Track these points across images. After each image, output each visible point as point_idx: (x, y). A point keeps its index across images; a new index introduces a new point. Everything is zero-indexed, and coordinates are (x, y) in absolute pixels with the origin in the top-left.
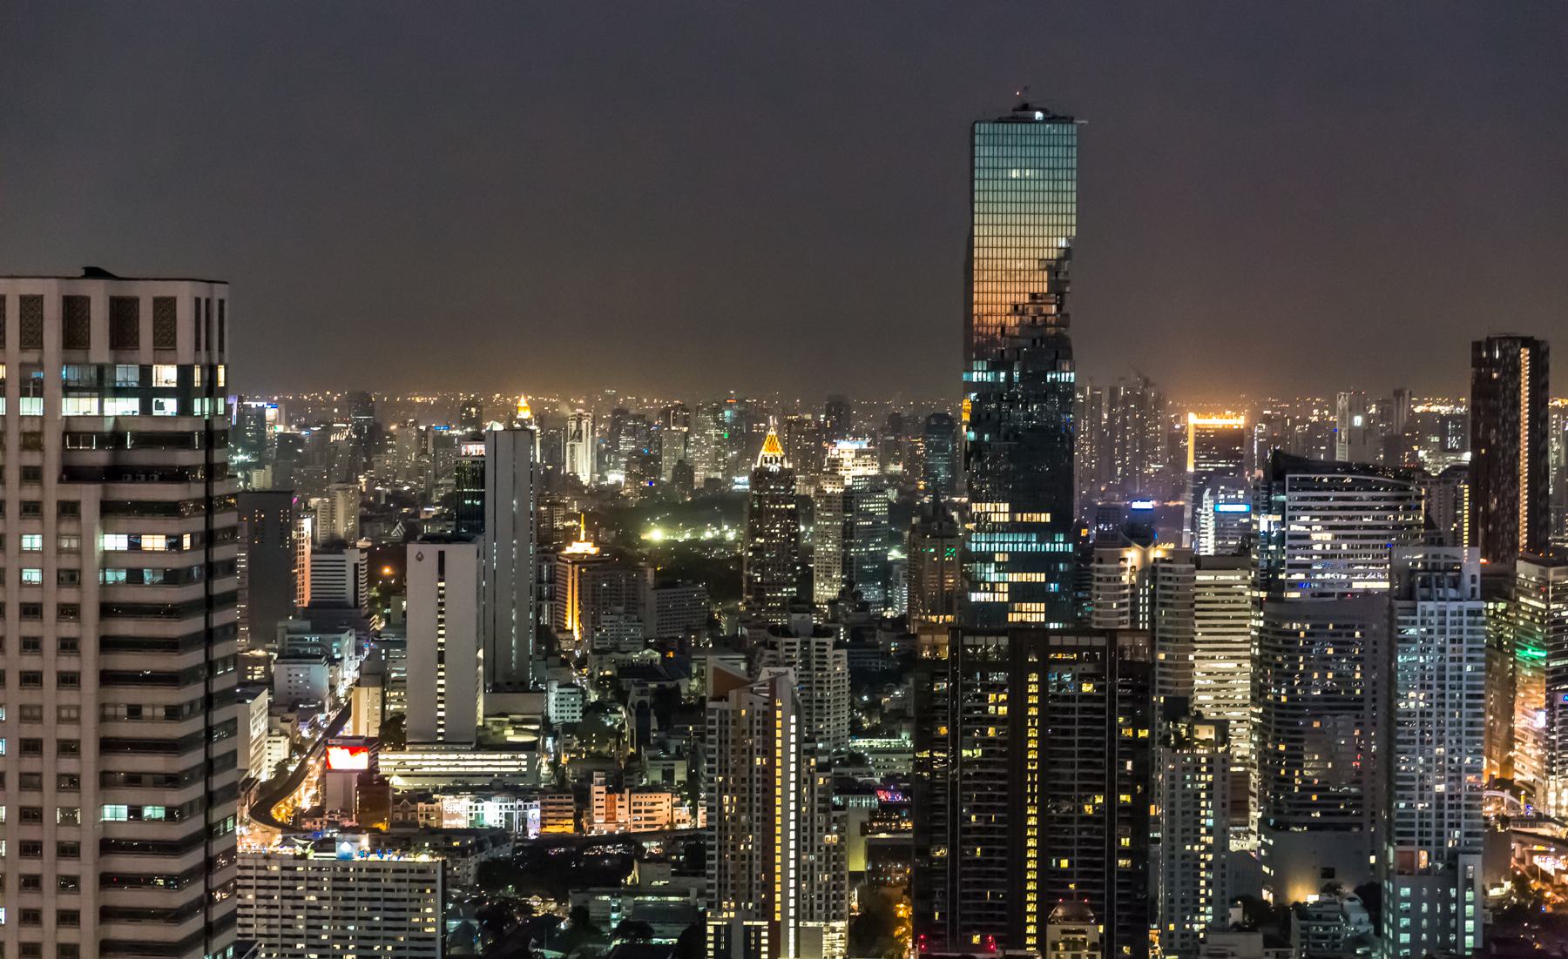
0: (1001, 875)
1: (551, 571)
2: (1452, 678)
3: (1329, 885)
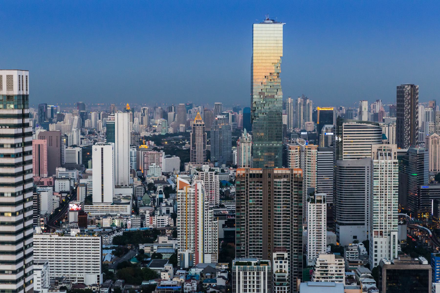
0: (260, 239)
1: (338, 153)
2: (389, 182)
3: (355, 241)
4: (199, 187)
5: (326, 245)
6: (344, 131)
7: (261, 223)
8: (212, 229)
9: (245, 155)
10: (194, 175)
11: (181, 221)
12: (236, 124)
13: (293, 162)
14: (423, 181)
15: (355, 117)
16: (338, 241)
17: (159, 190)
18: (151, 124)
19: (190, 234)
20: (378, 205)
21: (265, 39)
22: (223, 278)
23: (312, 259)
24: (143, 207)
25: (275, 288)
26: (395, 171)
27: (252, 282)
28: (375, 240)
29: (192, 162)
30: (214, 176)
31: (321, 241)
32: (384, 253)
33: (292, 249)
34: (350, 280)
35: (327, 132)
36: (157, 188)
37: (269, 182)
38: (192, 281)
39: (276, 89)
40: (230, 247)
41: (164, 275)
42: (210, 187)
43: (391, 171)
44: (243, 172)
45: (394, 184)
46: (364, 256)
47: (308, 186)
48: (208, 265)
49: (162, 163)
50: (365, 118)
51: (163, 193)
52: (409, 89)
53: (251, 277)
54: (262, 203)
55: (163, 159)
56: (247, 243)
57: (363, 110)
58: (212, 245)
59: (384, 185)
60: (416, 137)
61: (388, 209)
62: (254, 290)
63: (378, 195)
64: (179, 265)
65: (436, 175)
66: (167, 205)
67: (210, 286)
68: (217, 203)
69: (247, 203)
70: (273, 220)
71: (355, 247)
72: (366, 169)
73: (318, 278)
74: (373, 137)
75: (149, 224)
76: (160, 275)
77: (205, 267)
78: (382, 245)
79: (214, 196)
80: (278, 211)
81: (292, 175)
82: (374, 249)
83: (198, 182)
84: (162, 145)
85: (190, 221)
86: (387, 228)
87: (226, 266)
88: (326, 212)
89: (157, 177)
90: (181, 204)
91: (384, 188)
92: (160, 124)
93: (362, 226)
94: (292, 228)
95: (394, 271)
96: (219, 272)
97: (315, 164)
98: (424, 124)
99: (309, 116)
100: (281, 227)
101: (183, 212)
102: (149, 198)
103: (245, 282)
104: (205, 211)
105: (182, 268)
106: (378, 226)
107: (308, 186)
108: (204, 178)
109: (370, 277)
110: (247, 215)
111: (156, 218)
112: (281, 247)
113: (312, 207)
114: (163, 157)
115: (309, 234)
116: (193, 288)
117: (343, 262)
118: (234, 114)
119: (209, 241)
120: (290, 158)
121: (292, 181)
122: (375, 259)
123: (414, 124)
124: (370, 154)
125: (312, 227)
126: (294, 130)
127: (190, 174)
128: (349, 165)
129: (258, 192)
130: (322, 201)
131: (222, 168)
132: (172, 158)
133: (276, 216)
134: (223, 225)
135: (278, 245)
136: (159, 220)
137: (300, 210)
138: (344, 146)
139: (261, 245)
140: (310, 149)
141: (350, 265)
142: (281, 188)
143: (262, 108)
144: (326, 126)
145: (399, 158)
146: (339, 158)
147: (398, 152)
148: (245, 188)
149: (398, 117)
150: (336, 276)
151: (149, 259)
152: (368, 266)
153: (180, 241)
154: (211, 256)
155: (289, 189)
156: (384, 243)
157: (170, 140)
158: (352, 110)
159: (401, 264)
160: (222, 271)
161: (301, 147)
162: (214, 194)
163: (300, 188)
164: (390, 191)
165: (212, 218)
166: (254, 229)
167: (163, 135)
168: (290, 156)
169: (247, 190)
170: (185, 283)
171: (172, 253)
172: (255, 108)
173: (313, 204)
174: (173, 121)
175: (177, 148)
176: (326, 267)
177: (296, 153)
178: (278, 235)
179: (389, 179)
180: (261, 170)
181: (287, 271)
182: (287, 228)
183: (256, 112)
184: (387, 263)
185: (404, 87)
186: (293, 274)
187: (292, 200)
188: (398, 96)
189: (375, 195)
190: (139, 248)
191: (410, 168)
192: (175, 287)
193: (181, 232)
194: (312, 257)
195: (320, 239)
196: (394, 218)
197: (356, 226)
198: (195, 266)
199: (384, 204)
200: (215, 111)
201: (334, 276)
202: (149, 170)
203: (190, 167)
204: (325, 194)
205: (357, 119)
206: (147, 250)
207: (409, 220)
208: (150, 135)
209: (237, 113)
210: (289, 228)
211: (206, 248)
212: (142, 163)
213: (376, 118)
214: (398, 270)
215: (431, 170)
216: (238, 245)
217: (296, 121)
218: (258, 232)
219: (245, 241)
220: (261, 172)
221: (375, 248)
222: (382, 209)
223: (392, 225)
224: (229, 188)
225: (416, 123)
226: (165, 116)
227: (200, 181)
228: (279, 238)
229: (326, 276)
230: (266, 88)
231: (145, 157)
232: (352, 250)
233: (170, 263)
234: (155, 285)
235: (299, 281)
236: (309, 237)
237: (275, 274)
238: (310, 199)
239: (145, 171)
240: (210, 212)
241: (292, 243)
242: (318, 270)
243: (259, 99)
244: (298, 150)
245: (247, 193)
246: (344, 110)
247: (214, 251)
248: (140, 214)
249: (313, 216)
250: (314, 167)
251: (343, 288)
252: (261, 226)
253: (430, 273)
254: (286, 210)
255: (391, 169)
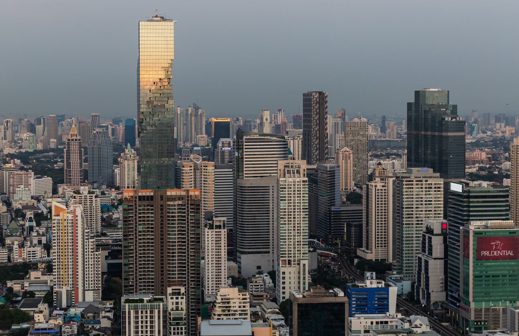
0: (152, 271)
1: (238, 171)
2: (298, 203)
4: (79, 211)
5: (226, 277)
6: (245, 145)
7: (152, 253)
8: (94, 261)
9: (128, 175)
10: (71, 199)
11: (58, 252)
12: (117, 139)
13: (186, 182)
14: (335, 202)
15: (254, 129)
16: (239, 272)
17: (29, 216)
18: (16, 139)
19: (68, 268)
20: (285, 230)
21: (154, 39)
22: (109, 318)
23: (210, 293)
24: (9, 238)
25: (170, 328)
26: (305, 191)
27: (144, 322)
28: (282, 270)
29: (67, 183)
30: (94, 199)
31: (221, 272)
32: (292, 285)
33: (188, 283)
34: (255, 317)
35: (223, 147)
36: (26, 214)
37: (162, 206)
38: (71, 323)
39: (166, 97)
40: (115, 282)
41: (38, 316)
42: (89, 212)
43: (300, 191)
44: (131, 194)
45: (303, 206)
46: (270, 288)
47: (204, 209)
48: (89, 304)
49: (31, 185)
50: (267, 130)
51: (34, 220)
52: (317, 96)
53: (144, 316)
54: (153, 230)
55: (32, 181)
56: (136, 277)
57: (264, 120)
58: (94, 281)
59: (292, 207)
60: (325, 152)
61: (296, 234)
62: (182, 333)
63: (286, 218)
64: (55, 305)
65: (347, 195)
66: (39, 234)
67: (93, 328)
68: (98, 230)
69: (136, 230)
70: (167, 249)
71: (260, 279)
72: (271, 188)
73: (219, 315)
74: (277, 152)
75: (18, 257)
76: (34, 317)
77: (86, 306)
78: (290, 275)
79: (95, 223)
80: (172, 238)
81: (188, 197)
82: (282, 281)
83: (76, 207)
84: (29, 164)
85: (68, 252)
86: (296, 257)
87: (110, 304)
88: (226, 239)
89: (26, 202)
90: (57, 233)
91: (292, 210)
92: (26, 140)
93: (266, 254)
94: (188, 258)
95: (307, 305)
96: (103, 312)
97: (212, 184)
98: (332, 138)
99: (201, 129)
100: (175, 257)
101: (59, 243)
102: (17, 227)
103: (137, 322)
104: (85, 241)
105: (58, 309)
106: (285, 254)
107: (204, 209)
108: (83, 202)
109: (278, 313)
110: (136, 245)
111: (26, 249)
112: (176, 281)
113: (210, 234)
114: (32, 178)
115: (207, 265)
116: (73, 331)
117: (248, 296)
118: (114, 127)
119: (90, 276)
120: (184, 177)
121: (188, 204)
122: (283, 292)
123: (322, 136)
124: (276, 171)
125: (210, 257)
126: (184, 145)
127: (64, 197)
128: (251, 184)
129: (148, 217)
130: (222, 226)
131: (102, 190)
132: (43, 179)
133: (170, 245)
134: (106, 256)
135: (173, 278)
136: (30, 252)
137: (197, 237)
138: (245, 163)
139: (152, 279)
140: (206, 166)
141: (254, 300)
142: (175, 212)
143: (151, 120)
144: (222, 140)
145: (309, 175)
146: (240, 177)
147: (307, 169)
148: (133, 213)
149: (305, 129)
150: (240, 312)
151: (20, 298)
152: (275, 300)
153: (56, 277)
154: (94, 293)
155: (184, 213)
156: (292, 273)
157: (39, 158)
158: (250, 121)
159: (314, 297)
160: (106, 310)
161: (196, 165)
162: (95, 221)
163: (197, 212)
164: (299, 213)
165: (93, 248)
166: (144, 260)
167: (31, 152)
168: (184, 174)
169: (136, 215)
170: (63, 326)
171: (46, 291)
172: (143, 119)
173: (212, 230)
174: (42, 136)
175: (48, 167)
176: (228, 303)
177: (191, 171)
178: (173, 267)
179: (298, 200)
180: (152, 191)
181: (184, 308)
182: (183, 258)
183: (144, 124)
184: (298, 296)
185: (311, 95)
186: (190, 311)
187: (188, 225)
188: (304, 105)
189: (282, 218)
190: (6, 286)
191: (320, 187)
192: (51, 331)
193: (58, 265)
194: (210, 292)
195: (220, 271)
196: (303, 245)
197: (260, 255)
198: (74, 306)
199: (292, 228)
200: (92, 123)
201: (237, 313)
202: (15, 193)
203: (64, 189)
204: (225, 219)
205: (256, 131)
206: (17, 288)
207: (319, 246)
208: (15, 152)
209: (117, 126)
210: (185, 258)
211: (87, 284)
212: (7, 185)
213: (278, 130)
214: (311, 304)
215: (342, 189)
216: (125, 279)
217: (187, 135)
218: (148, 264)
219: (134, 274)
220: (152, 194)
221: (283, 279)
222: (290, 234)
223: (302, 252)
224: (111, 213)
225: (325, 135)
226: (32, 129)
227: (78, 205)
228: (173, 271)
229: (229, 313)
230: (154, 96)
231: (11, 178)
232: (256, 282)
233: (44, 302)
234: (28, 329)
235: (199, 319)
236: (207, 268)
237: (170, 313)
238: (208, 225)
239: (11, 195)
240: (91, 242)
241: (188, 276)
242: (219, 307)
243: (147, 108)
244: (193, 168)
245: (135, 219)
246: (241, 121)
247: (97, 287)
248: (7, 245)
249: (212, 244)
250: (211, 187)
251: (251, 326)
252: (152, 257)
253: (347, 306)
254: (181, 237)
255: (300, 188)
